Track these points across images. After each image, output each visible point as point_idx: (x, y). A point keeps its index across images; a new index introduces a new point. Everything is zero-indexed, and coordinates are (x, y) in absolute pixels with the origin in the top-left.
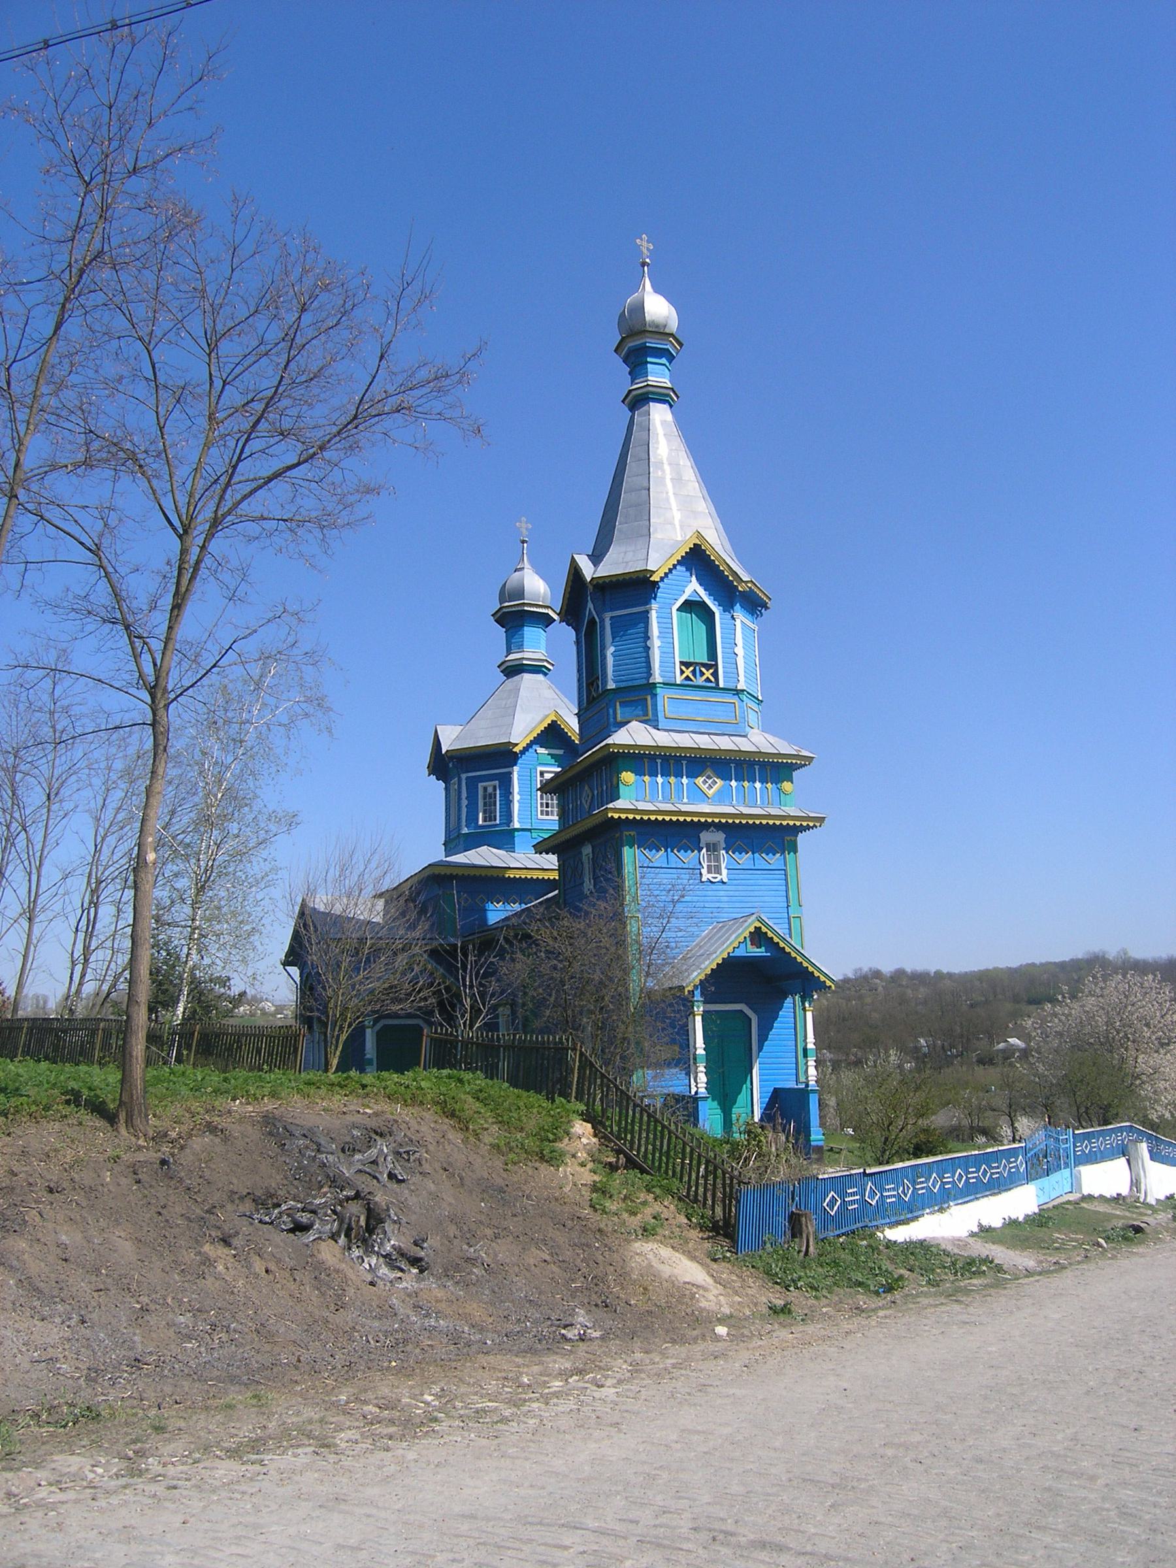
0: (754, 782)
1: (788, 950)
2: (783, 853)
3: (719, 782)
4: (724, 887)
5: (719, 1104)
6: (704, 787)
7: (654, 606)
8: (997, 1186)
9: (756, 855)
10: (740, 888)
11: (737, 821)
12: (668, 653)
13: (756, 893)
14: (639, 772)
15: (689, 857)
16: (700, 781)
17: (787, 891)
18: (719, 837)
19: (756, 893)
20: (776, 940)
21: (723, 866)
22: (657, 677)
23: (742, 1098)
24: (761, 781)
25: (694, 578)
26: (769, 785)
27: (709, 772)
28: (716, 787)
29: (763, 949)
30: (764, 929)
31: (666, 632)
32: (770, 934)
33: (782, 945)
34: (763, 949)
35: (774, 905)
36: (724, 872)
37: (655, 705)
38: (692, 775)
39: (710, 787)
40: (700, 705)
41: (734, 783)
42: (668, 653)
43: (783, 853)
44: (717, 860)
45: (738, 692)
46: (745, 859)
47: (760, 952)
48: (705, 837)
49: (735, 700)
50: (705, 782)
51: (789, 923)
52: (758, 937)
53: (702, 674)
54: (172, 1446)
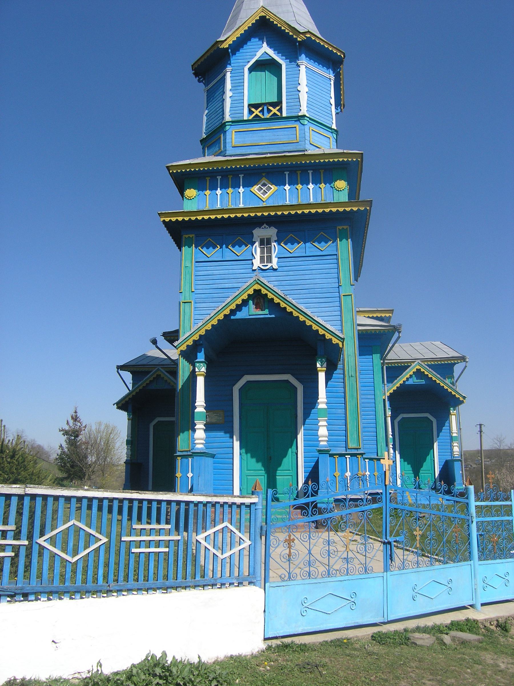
0: (308, 184)
1: (289, 309)
2: (335, 241)
3: (274, 188)
4: (276, 273)
5: (263, 465)
6: (259, 194)
7: (229, 68)
8: (181, 572)
9: (308, 244)
10: (291, 273)
11: (279, 213)
12: (237, 102)
13: (307, 277)
14: (201, 188)
15: (240, 251)
16: (255, 189)
17: (338, 273)
18: (271, 232)
19: (307, 277)
20: (276, 301)
21: (274, 255)
22: (228, 118)
23: (287, 462)
24: (315, 182)
25: (265, 44)
26: (322, 185)
27: (264, 181)
28: (269, 193)
29: (266, 311)
30: (264, 291)
31: (238, 86)
32: (270, 296)
33: (283, 305)
34: (266, 311)
35: (325, 286)
36: (275, 260)
37: (225, 139)
38: (248, 184)
39: (265, 193)
40: (264, 134)
41: (287, 187)
42: (237, 102)
43: (335, 241)
44: (269, 251)
45: (299, 118)
46: (296, 249)
47: (264, 313)
48: (259, 233)
49: (297, 125)
50: (260, 189)
51: (340, 301)
52: (258, 298)
53: (269, 111)
54: (501, 664)
